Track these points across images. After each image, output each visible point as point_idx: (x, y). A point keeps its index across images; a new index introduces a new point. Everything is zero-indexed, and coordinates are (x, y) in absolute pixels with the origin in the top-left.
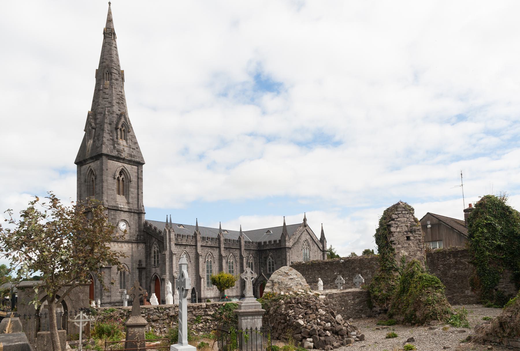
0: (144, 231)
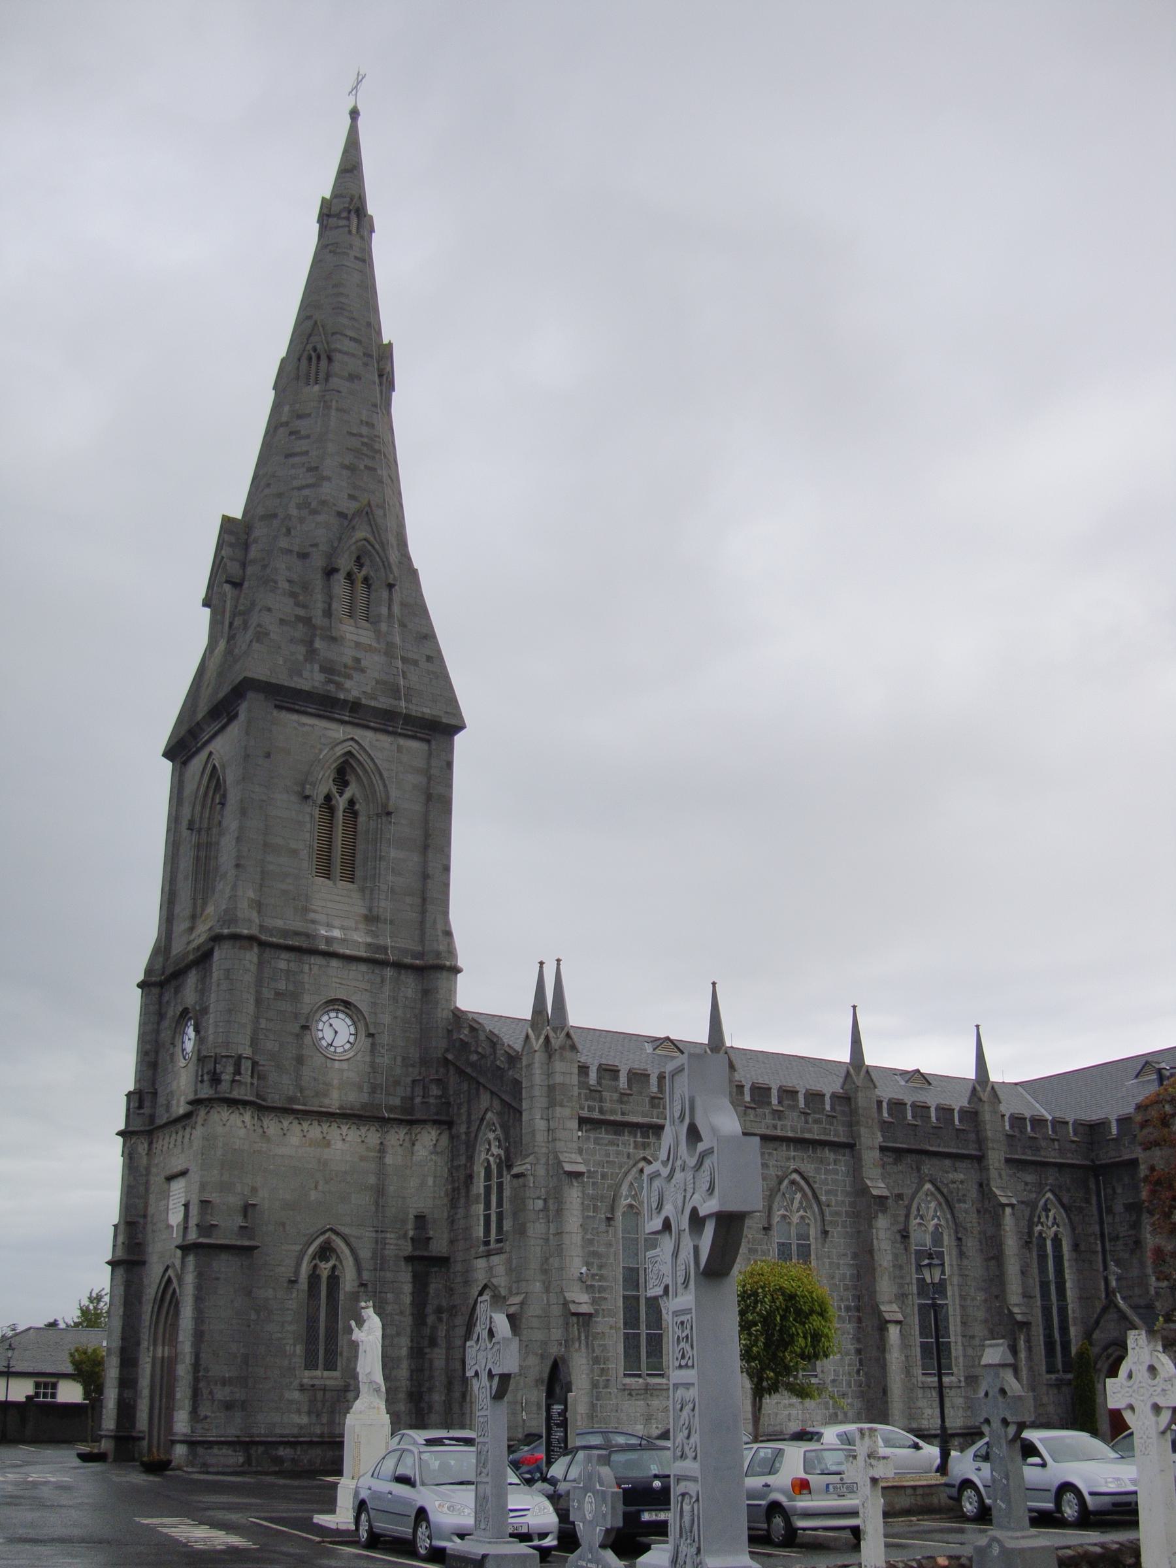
0: (446, 1059)
